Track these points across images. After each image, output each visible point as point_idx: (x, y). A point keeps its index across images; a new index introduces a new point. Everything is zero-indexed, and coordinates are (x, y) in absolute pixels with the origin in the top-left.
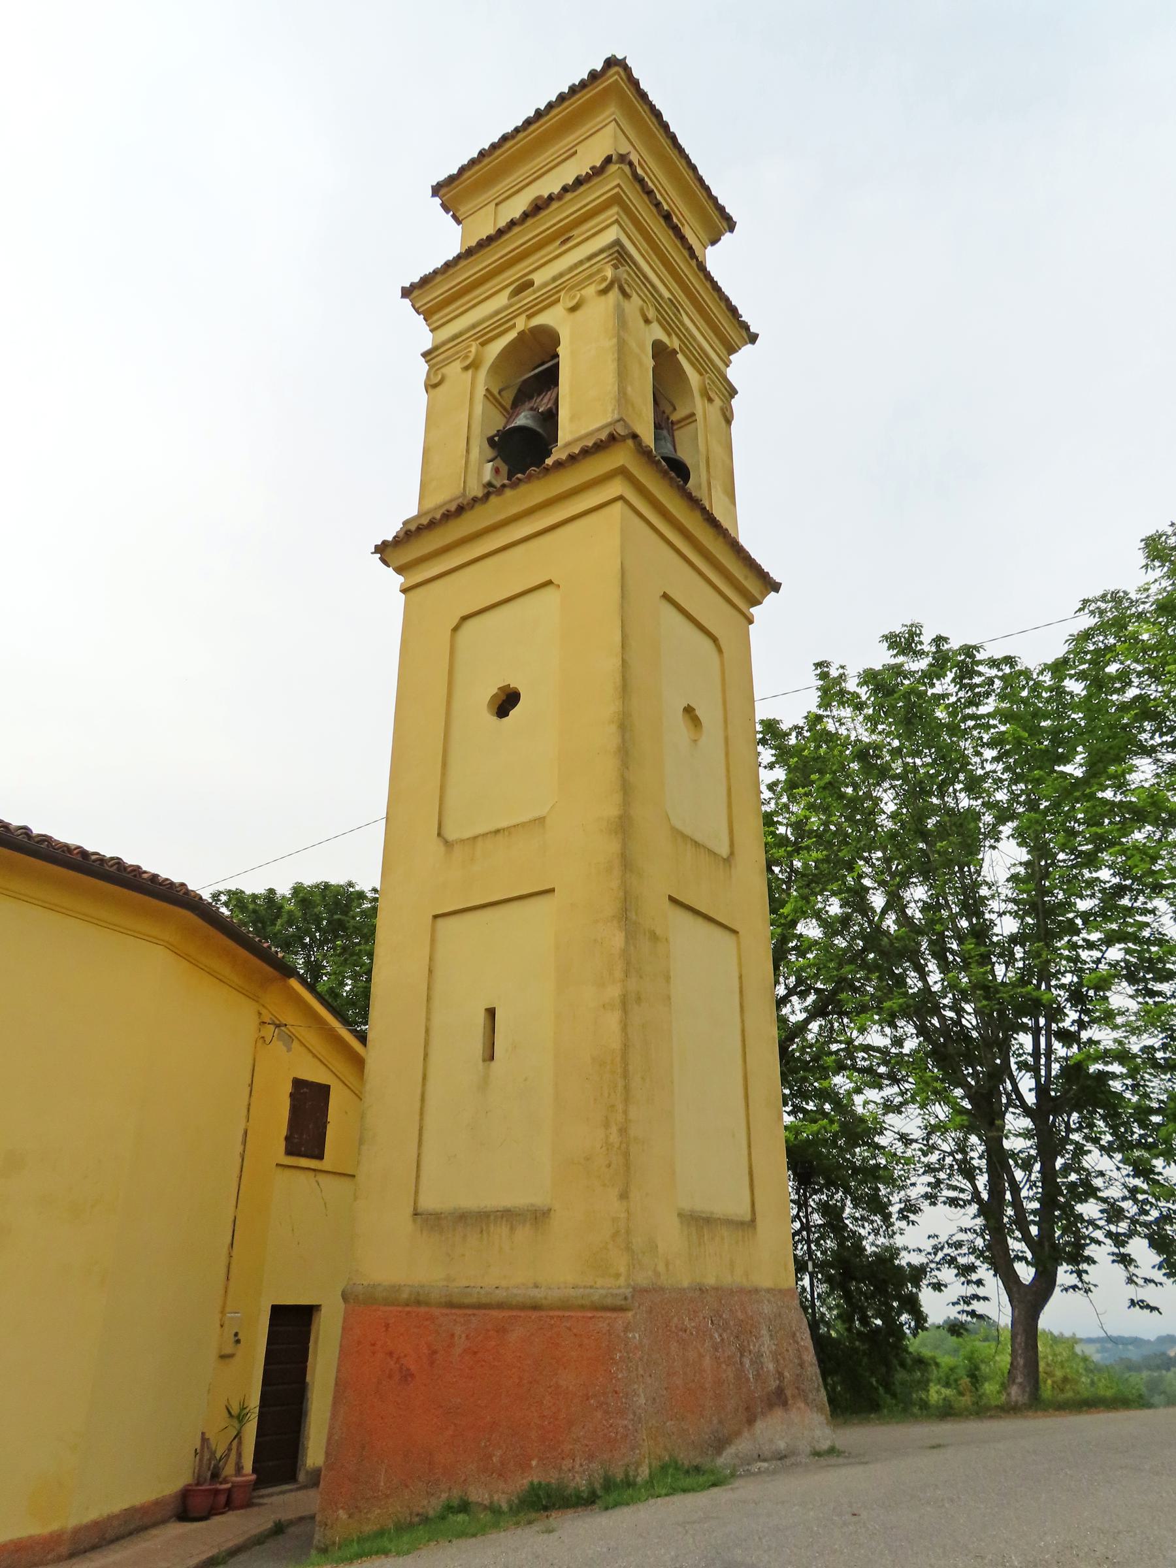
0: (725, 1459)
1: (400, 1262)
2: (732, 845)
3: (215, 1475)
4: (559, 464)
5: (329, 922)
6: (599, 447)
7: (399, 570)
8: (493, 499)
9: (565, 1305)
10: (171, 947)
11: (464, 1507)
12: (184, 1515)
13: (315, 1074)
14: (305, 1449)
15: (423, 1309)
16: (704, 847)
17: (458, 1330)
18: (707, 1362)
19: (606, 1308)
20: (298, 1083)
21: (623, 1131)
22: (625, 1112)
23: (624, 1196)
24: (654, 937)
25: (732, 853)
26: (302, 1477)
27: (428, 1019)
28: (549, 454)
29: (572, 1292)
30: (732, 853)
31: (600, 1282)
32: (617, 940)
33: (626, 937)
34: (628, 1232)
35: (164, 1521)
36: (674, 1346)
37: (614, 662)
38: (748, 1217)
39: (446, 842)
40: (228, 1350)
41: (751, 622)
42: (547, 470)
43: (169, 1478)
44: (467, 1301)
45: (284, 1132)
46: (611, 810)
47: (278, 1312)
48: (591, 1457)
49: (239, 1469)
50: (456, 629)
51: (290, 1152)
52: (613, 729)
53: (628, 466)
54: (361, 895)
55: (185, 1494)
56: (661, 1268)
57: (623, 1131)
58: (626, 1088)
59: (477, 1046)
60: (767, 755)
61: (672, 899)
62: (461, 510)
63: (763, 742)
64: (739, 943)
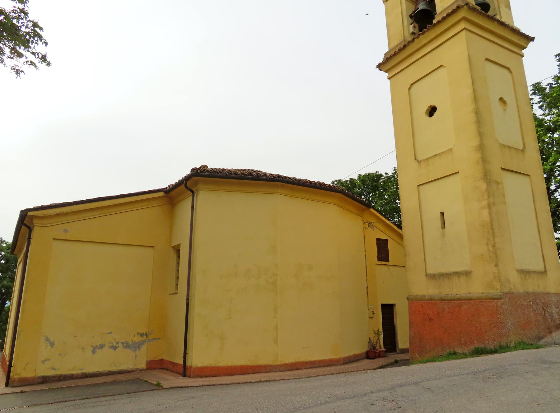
0: (542, 342)
1: (423, 288)
2: (524, 144)
3: (374, 348)
4: (439, 22)
5: (372, 186)
6: (454, 12)
7: (386, 72)
8: (416, 40)
9: (479, 299)
10: (336, 204)
11: (455, 353)
12: (368, 358)
13: (384, 237)
14: (398, 343)
15: (433, 301)
16: (513, 148)
17: (445, 307)
18: (532, 314)
19: (493, 299)
20: (378, 240)
21: (494, 246)
22: (494, 240)
23: (496, 266)
24: (497, 183)
25: (524, 147)
26: (398, 351)
27: (421, 217)
28: (434, 18)
29: (482, 295)
30: (524, 147)
31: (491, 291)
32: (484, 186)
33: (487, 185)
34: (499, 277)
35: (363, 359)
36: (519, 310)
37: (470, 91)
38: (543, 270)
39: (418, 161)
40: (372, 316)
41: (523, 56)
42: (435, 25)
43: (363, 349)
44: (448, 298)
45: (376, 254)
46: (475, 142)
47: (384, 306)
48: (494, 340)
49: (380, 347)
50: (409, 89)
51: (379, 260)
52: (473, 115)
53: (467, 16)
54: (381, 175)
55: (367, 352)
56: (512, 287)
57: (494, 246)
58: (493, 233)
59: (439, 224)
60: (536, 98)
61: (502, 169)
62: (405, 47)
63: (534, 93)
64: (531, 180)
